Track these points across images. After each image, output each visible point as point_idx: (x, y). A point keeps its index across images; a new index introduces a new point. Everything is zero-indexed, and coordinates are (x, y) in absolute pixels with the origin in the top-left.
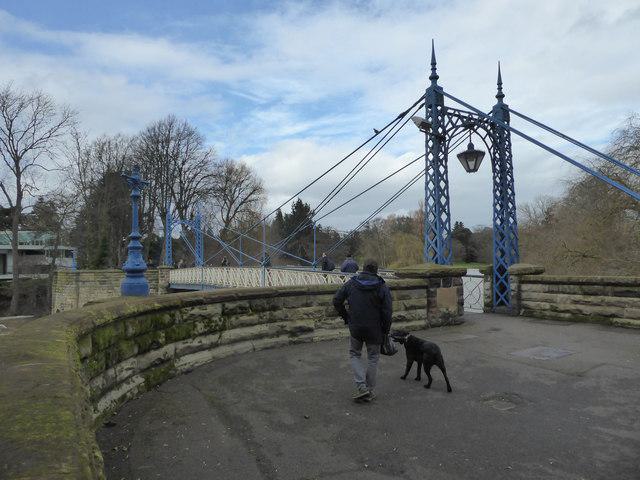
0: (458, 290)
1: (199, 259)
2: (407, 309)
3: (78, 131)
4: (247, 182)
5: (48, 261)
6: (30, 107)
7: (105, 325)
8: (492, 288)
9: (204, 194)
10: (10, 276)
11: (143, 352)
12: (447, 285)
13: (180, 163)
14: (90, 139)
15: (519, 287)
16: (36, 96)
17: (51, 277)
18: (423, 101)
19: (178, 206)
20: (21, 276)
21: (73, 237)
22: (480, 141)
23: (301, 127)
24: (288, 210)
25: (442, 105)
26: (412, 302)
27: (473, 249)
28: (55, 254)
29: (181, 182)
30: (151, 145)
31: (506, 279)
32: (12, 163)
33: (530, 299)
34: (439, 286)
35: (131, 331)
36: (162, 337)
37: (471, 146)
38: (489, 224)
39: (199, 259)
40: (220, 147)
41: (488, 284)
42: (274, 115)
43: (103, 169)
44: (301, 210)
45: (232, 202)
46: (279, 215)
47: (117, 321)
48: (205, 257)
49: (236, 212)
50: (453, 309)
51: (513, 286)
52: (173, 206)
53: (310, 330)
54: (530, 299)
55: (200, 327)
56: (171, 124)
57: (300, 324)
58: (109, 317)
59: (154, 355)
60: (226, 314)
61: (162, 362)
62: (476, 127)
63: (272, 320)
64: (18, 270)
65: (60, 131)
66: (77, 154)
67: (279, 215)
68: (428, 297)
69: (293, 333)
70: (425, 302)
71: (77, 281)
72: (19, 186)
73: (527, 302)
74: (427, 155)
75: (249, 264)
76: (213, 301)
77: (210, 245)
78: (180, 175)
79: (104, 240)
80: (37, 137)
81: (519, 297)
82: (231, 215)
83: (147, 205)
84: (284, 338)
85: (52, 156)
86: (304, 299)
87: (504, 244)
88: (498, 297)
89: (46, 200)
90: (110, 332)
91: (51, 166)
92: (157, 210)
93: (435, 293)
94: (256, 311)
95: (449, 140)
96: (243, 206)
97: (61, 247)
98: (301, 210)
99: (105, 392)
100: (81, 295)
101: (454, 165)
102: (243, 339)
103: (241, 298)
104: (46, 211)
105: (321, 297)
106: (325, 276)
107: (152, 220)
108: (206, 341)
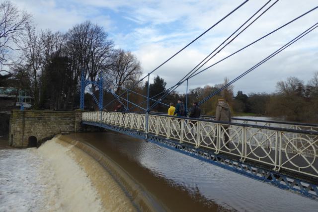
1: (101, 107)
4: (131, 63)
9: (106, 68)
14: (38, 34)
23: (161, 38)
24: (152, 82)
27: (249, 105)
29: (93, 60)
30: (77, 39)
39: (101, 107)
40: (119, 43)
42: (147, 31)
44: (159, 82)
45: (122, 75)
48: (104, 105)
49: (124, 80)
56: (88, 26)
66: (29, 40)
71: (24, 117)
75: (133, 110)
77: (108, 96)
80: (7, 30)
82: (122, 82)
85: (16, 41)
91: (15, 46)
96: (128, 77)
98: (159, 82)
100: (26, 126)
106: (179, 120)
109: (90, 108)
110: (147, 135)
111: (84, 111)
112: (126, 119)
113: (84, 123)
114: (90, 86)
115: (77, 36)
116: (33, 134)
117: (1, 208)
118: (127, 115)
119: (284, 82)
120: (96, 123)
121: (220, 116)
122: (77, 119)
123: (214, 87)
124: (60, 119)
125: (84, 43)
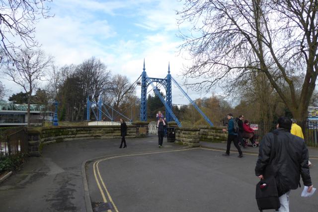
3: (55, 65)
4: (127, 84)
5: (42, 117)
6: (36, 55)
7: (48, 129)
10: (26, 124)
11: (56, 136)
12: (143, 126)
13: (96, 77)
16: (38, 51)
17: (249, 146)
20: (31, 124)
21: (53, 107)
28: (45, 115)
32: (28, 78)
35: (54, 131)
36: (61, 134)
43: (65, 78)
47: (50, 129)
50: (144, 133)
53: (100, 136)
55: (70, 133)
57: (97, 134)
58: (49, 128)
59: (58, 137)
60: (77, 131)
61: (62, 139)
63: (90, 133)
64: (30, 121)
65: (48, 64)
69: (95, 136)
72: (31, 87)
76: (74, 128)
79: (64, 110)
84: (93, 137)
86: (99, 129)
89: (42, 90)
90: (49, 131)
94: (85, 131)
97: (47, 112)
99: (48, 140)
102: (81, 137)
103: (81, 128)
104: (42, 96)
105: (103, 129)
108: (72, 136)
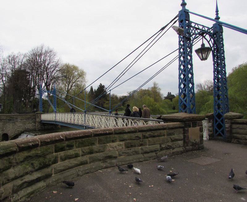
0: (200, 128)
2: (172, 141)
8: (213, 126)
12: (195, 125)
15: (231, 127)
18: (177, 18)
19: (46, 84)
22: (208, 41)
24: (95, 88)
25: (189, 20)
26: (176, 136)
29: (47, 73)
31: (222, 121)
33: (238, 133)
34: (190, 127)
37: (203, 45)
38: (175, 92)
41: (210, 124)
46: (92, 89)
49: (71, 86)
50: (198, 140)
51: (227, 125)
52: (43, 85)
54: (238, 133)
62: (204, 35)
67: (92, 89)
68: (184, 133)
70: (182, 136)
73: (235, 135)
74: (180, 49)
78: (47, 70)
81: (231, 132)
82: (70, 87)
83: (32, 84)
87: (186, 101)
88: (217, 131)
92: (36, 86)
93: (188, 131)
95: (193, 40)
98: (101, 88)
101: (195, 58)
107: (34, 91)
109: (46, 111)
110: (85, 127)
111: (42, 113)
112: (76, 117)
113: (42, 122)
114: (46, 94)
115: (35, 55)
116: (5, 132)
117: (2, 189)
118: (77, 115)
119: (202, 84)
120: (52, 121)
121: (240, 139)
122: (38, 120)
123: (147, 89)
124: (25, 120)
125: (40, 60)
